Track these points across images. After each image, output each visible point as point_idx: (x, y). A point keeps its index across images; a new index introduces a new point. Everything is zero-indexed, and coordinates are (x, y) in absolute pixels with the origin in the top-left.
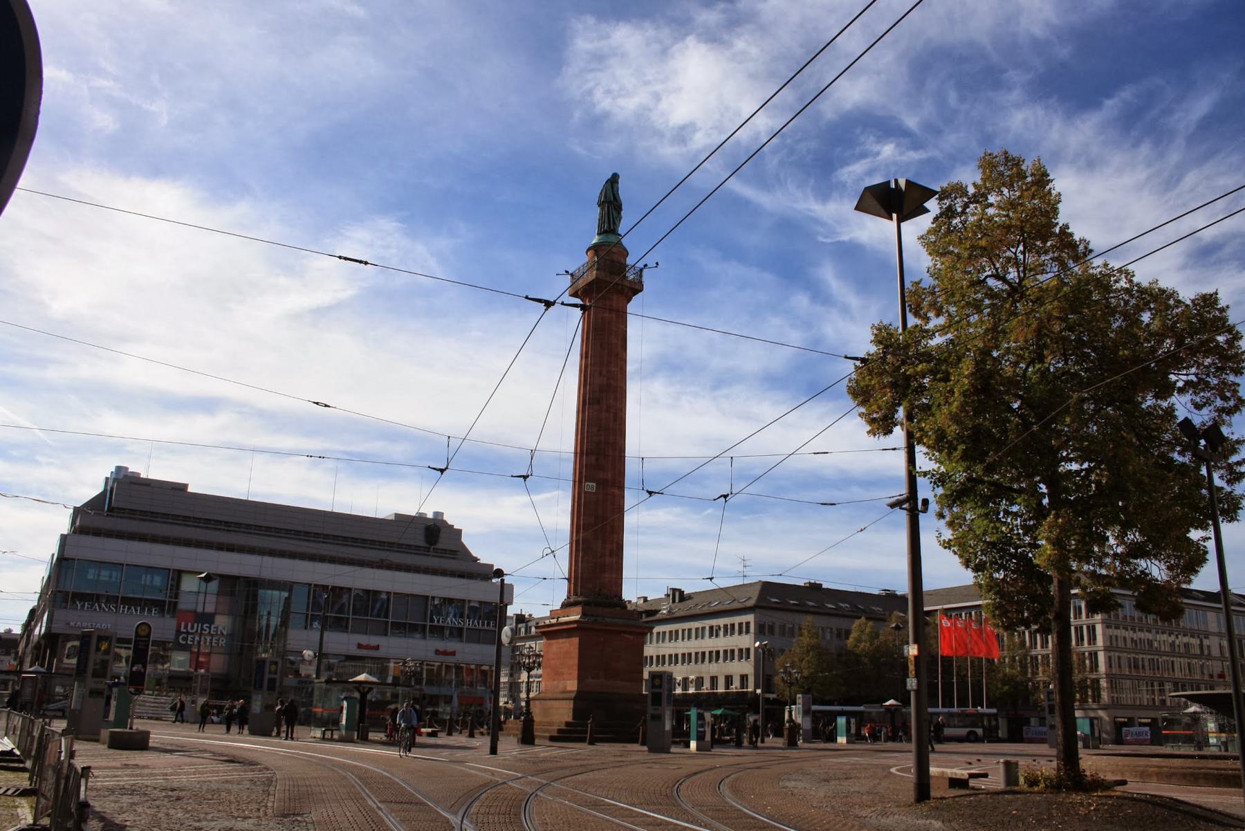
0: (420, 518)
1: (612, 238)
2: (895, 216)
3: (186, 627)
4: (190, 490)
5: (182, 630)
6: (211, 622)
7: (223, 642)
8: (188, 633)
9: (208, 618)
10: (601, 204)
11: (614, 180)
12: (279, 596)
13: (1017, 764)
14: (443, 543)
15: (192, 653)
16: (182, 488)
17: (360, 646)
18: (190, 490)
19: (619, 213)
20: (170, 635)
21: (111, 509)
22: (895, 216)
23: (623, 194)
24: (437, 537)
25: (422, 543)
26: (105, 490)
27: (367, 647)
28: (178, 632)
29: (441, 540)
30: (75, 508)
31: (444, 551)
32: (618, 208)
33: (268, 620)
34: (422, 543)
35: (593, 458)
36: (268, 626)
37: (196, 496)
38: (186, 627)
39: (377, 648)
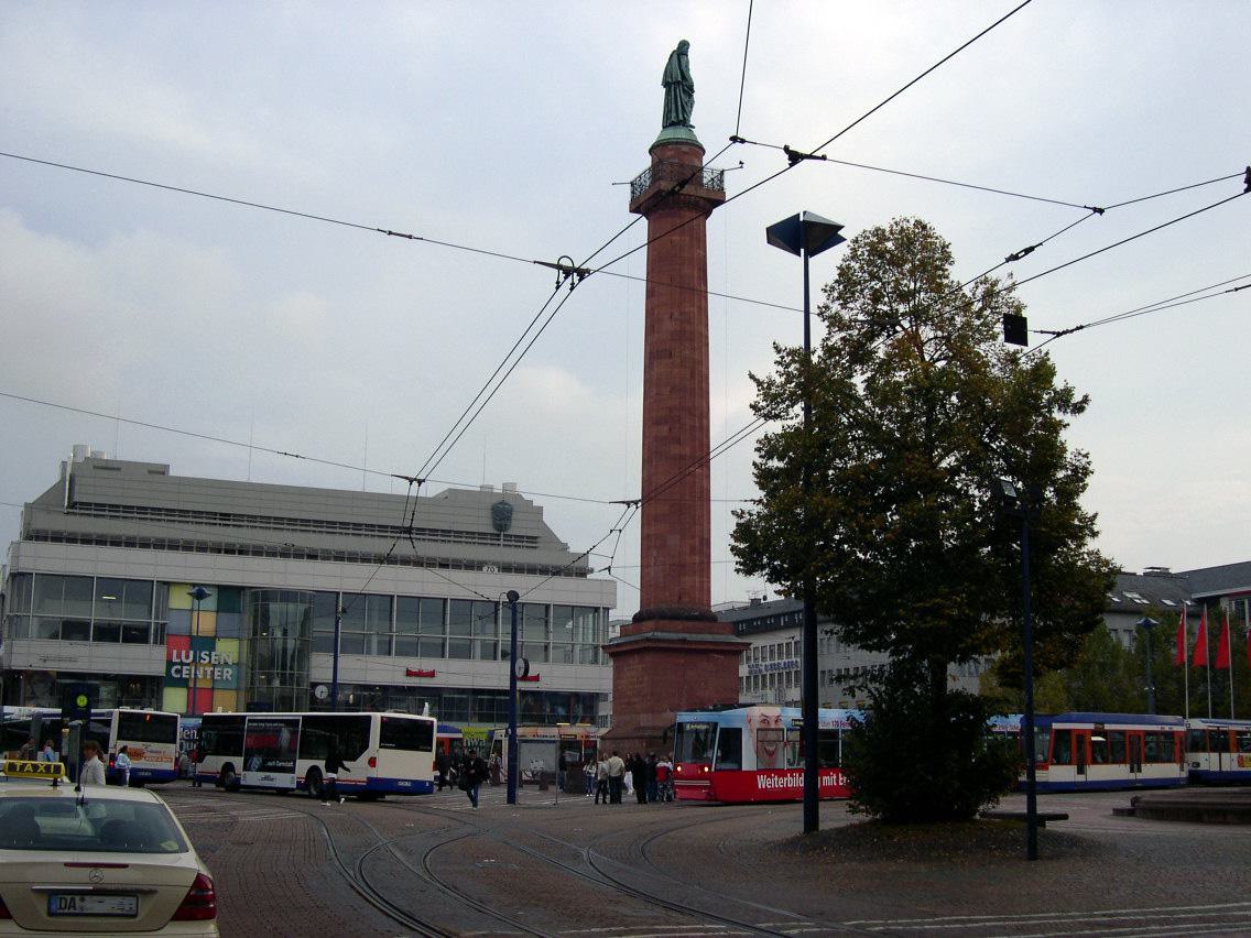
0: (486, 492)
1: (680, 133)
2: (802, 251)
3: (179, 656)
4: (172, 473)
5: (175, 660)
6: (213, 648)
7: (229, 673)
8: (182, 664)
9: (208, 643)
10: (666, 84)
11: (682, 50)
12: (295, 610)
13: (721, 729)
14: (516, 528)
15: (189, 689)
16: (161, 471)
17: (409, 673)
18: (172, 473)
19: (691, 96)
20: (158, 669)
21: (72, 505)
22: (802, 251)
23: (695, 73)
24: (509, 518)
25: (491, 530)
26: (63, 478)
27: (420, 674)
28: (170, 663)
29: (514, 523)
30: (27, 506)
31: (520, 538)
32: (689, 91)
33: (285, 643)
34: (491, 530)
35: (665, 429)
36: (285, 650)
37: (181, 481)
38: (179, 656)
39: (432, 674)
